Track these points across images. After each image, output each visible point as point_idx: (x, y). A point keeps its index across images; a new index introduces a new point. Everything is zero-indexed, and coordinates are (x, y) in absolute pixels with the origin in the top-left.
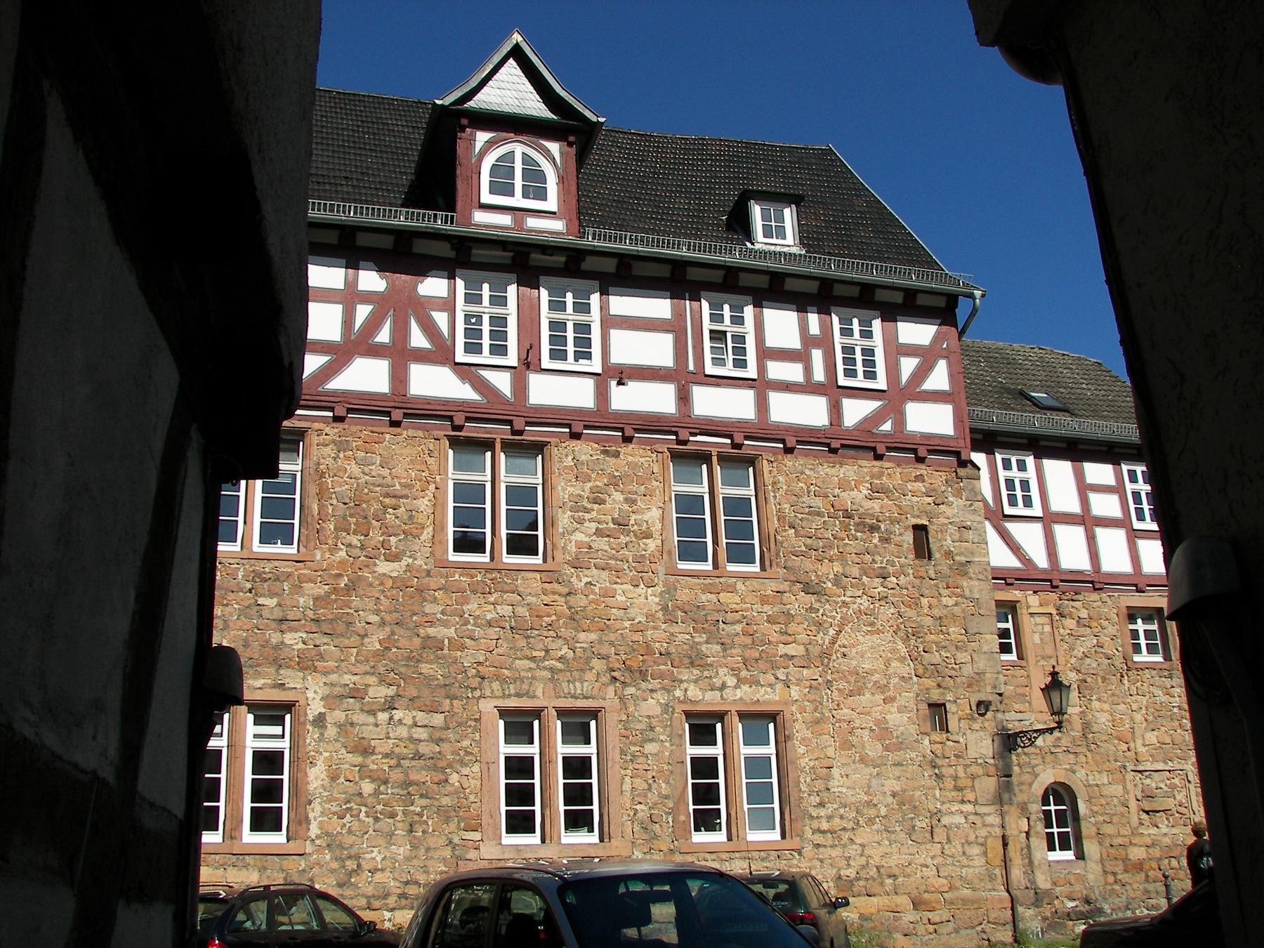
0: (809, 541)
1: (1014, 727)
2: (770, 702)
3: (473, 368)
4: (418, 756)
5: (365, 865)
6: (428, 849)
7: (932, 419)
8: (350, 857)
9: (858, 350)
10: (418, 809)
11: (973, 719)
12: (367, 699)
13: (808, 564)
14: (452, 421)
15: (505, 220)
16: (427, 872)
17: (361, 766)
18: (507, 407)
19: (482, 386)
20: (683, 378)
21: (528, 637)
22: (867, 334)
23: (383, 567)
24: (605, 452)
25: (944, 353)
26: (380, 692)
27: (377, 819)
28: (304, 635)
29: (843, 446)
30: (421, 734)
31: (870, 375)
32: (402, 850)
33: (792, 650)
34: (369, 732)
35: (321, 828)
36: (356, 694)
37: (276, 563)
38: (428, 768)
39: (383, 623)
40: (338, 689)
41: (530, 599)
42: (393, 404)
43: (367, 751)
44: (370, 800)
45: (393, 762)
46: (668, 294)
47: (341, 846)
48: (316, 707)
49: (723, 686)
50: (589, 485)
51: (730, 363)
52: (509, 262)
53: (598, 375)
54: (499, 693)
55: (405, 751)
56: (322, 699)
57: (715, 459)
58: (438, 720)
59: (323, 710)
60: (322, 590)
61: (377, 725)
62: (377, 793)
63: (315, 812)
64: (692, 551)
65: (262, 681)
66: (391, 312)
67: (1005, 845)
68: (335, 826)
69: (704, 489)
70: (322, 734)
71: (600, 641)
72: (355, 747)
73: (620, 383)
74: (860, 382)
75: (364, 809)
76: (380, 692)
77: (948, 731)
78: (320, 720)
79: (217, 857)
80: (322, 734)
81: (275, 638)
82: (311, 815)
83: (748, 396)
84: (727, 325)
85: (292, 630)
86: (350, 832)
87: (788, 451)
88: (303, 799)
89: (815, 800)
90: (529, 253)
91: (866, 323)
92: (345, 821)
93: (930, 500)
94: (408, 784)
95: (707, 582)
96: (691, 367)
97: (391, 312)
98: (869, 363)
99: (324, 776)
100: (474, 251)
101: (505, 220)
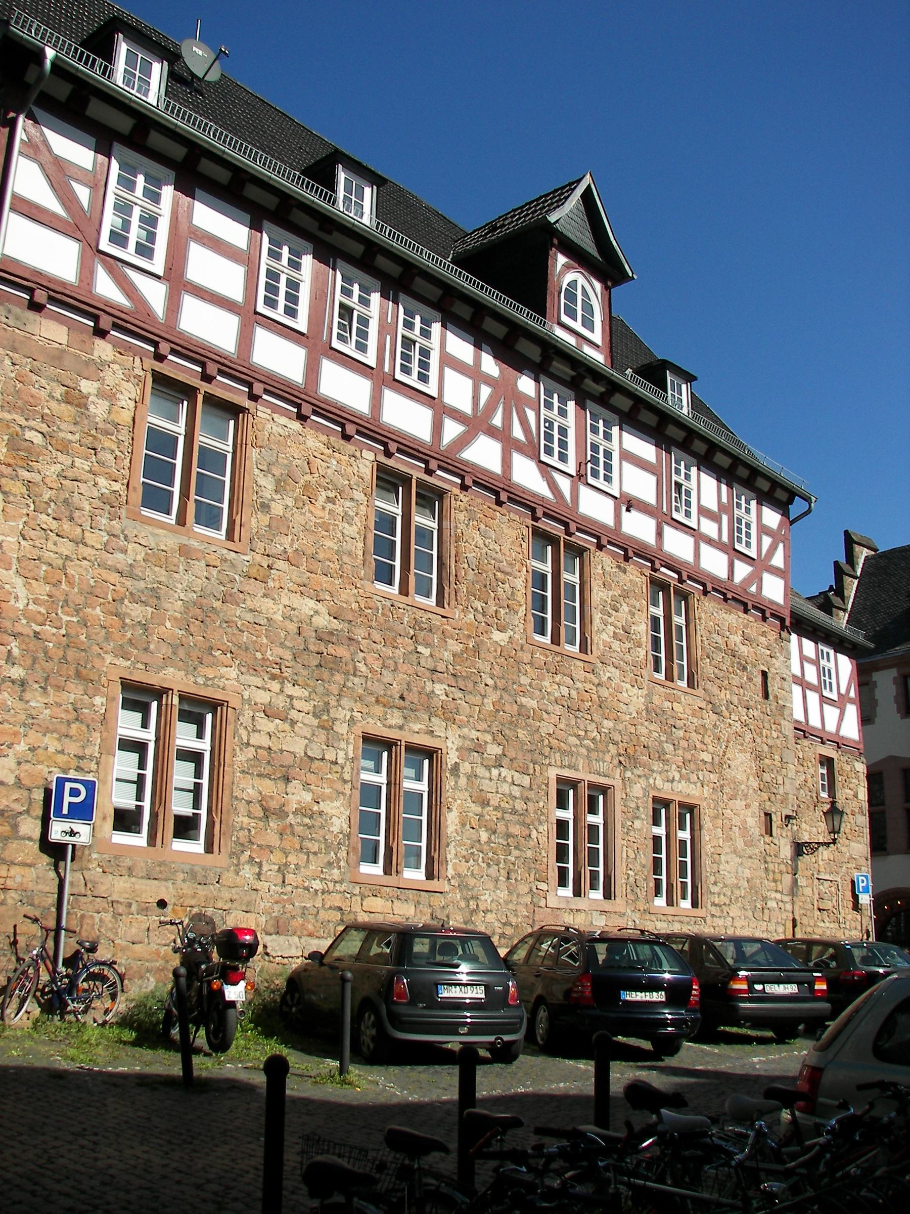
0: (716, 670)
1: (806, 838)
2: (693, 797)
3: (549, 469)
4: (514, 812)
5: (482, 907)
6: (518, 895)
7: (773, 590)
8: (472, 898)
9: (283, 278)
10: (513, 859)
11: (782, 828)
12: (485, 755)
13: (715, 690)
14: (32, 296)
15: (571, 340)
16: (516, 915)
17: (481, 816)
18: (564, 509)
19: (553, 486)
20: (476, 424)
21: (576, 717)
22: (295, 265)
23: (497, 636)
24: (619, 567)
25: (782, 538)
26: (494, 750)
27: (489, 865)
28: (447, 688)
29: (734, 599)
30: (516, 791)
31: (291, 312)
32: (503, 894)
33: (707, 757)
34: (486, 785)
35: (455, 870)
36: (479, 748)
37: (430, 615)
38: (519, 823)
39: (496, 687)
40: (467, 742)
41: (579, 685)
42: (502, 486)
43: (485, 803)
44: (486, 847)
45: (499, 815)
46: (715, 475)
47: (466, 886)
48: (452, 758)
49: (673, 781)
50: (610, 593)
51: (415, 375)
52: (569, 379)
53: (616, 498)
54: (559, 763)
55: (507, 806)
56: (457, 750)
57: (200, 398)
58: (526, 781)
59: (458, 761)
60: (458, 648)
61: (491, 779)
62: (489, 841)
63: (451, 853)
64: (157, 500)
65: (419, 726)
66: (502, 400)
67: (794, 926)
68: (463, 868)
69: (180, 428)
70: (456, 782)
71: (615, 729)
72: (478, 797)
73: (628, 510)
74: (278, 314)
75: (481, 855)
76: (494, 750)
77: (771, 835)
78: (456, 768)
79: (388, 889)
80: (456, 782)
81: (429, 687)
82: (449, 857)
83: (232, 322)
84: (353, 301)
85: (441, 682)
86: (472, 875)
87: (35, 307)
88: (443, 841)
89: (712, 879)
90: (585, 378)
91: (426, 322)
92: (469, 864)
93: (768, 652)
94: (508, 835)
95: (668, 691)
96: (665, 509)
97: (502, 400)
98: (293, 298)
99: (457, 821)
100: (554, 363)
101: (571, 340)
